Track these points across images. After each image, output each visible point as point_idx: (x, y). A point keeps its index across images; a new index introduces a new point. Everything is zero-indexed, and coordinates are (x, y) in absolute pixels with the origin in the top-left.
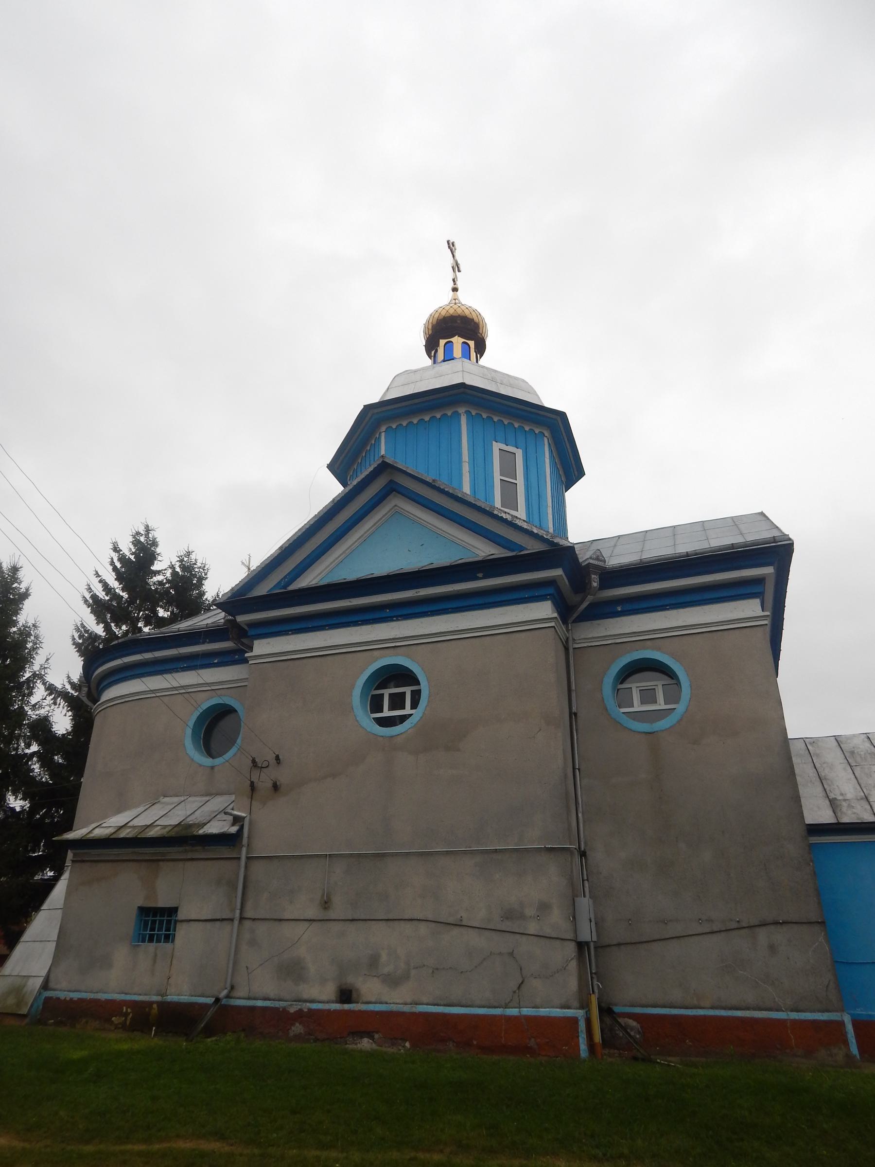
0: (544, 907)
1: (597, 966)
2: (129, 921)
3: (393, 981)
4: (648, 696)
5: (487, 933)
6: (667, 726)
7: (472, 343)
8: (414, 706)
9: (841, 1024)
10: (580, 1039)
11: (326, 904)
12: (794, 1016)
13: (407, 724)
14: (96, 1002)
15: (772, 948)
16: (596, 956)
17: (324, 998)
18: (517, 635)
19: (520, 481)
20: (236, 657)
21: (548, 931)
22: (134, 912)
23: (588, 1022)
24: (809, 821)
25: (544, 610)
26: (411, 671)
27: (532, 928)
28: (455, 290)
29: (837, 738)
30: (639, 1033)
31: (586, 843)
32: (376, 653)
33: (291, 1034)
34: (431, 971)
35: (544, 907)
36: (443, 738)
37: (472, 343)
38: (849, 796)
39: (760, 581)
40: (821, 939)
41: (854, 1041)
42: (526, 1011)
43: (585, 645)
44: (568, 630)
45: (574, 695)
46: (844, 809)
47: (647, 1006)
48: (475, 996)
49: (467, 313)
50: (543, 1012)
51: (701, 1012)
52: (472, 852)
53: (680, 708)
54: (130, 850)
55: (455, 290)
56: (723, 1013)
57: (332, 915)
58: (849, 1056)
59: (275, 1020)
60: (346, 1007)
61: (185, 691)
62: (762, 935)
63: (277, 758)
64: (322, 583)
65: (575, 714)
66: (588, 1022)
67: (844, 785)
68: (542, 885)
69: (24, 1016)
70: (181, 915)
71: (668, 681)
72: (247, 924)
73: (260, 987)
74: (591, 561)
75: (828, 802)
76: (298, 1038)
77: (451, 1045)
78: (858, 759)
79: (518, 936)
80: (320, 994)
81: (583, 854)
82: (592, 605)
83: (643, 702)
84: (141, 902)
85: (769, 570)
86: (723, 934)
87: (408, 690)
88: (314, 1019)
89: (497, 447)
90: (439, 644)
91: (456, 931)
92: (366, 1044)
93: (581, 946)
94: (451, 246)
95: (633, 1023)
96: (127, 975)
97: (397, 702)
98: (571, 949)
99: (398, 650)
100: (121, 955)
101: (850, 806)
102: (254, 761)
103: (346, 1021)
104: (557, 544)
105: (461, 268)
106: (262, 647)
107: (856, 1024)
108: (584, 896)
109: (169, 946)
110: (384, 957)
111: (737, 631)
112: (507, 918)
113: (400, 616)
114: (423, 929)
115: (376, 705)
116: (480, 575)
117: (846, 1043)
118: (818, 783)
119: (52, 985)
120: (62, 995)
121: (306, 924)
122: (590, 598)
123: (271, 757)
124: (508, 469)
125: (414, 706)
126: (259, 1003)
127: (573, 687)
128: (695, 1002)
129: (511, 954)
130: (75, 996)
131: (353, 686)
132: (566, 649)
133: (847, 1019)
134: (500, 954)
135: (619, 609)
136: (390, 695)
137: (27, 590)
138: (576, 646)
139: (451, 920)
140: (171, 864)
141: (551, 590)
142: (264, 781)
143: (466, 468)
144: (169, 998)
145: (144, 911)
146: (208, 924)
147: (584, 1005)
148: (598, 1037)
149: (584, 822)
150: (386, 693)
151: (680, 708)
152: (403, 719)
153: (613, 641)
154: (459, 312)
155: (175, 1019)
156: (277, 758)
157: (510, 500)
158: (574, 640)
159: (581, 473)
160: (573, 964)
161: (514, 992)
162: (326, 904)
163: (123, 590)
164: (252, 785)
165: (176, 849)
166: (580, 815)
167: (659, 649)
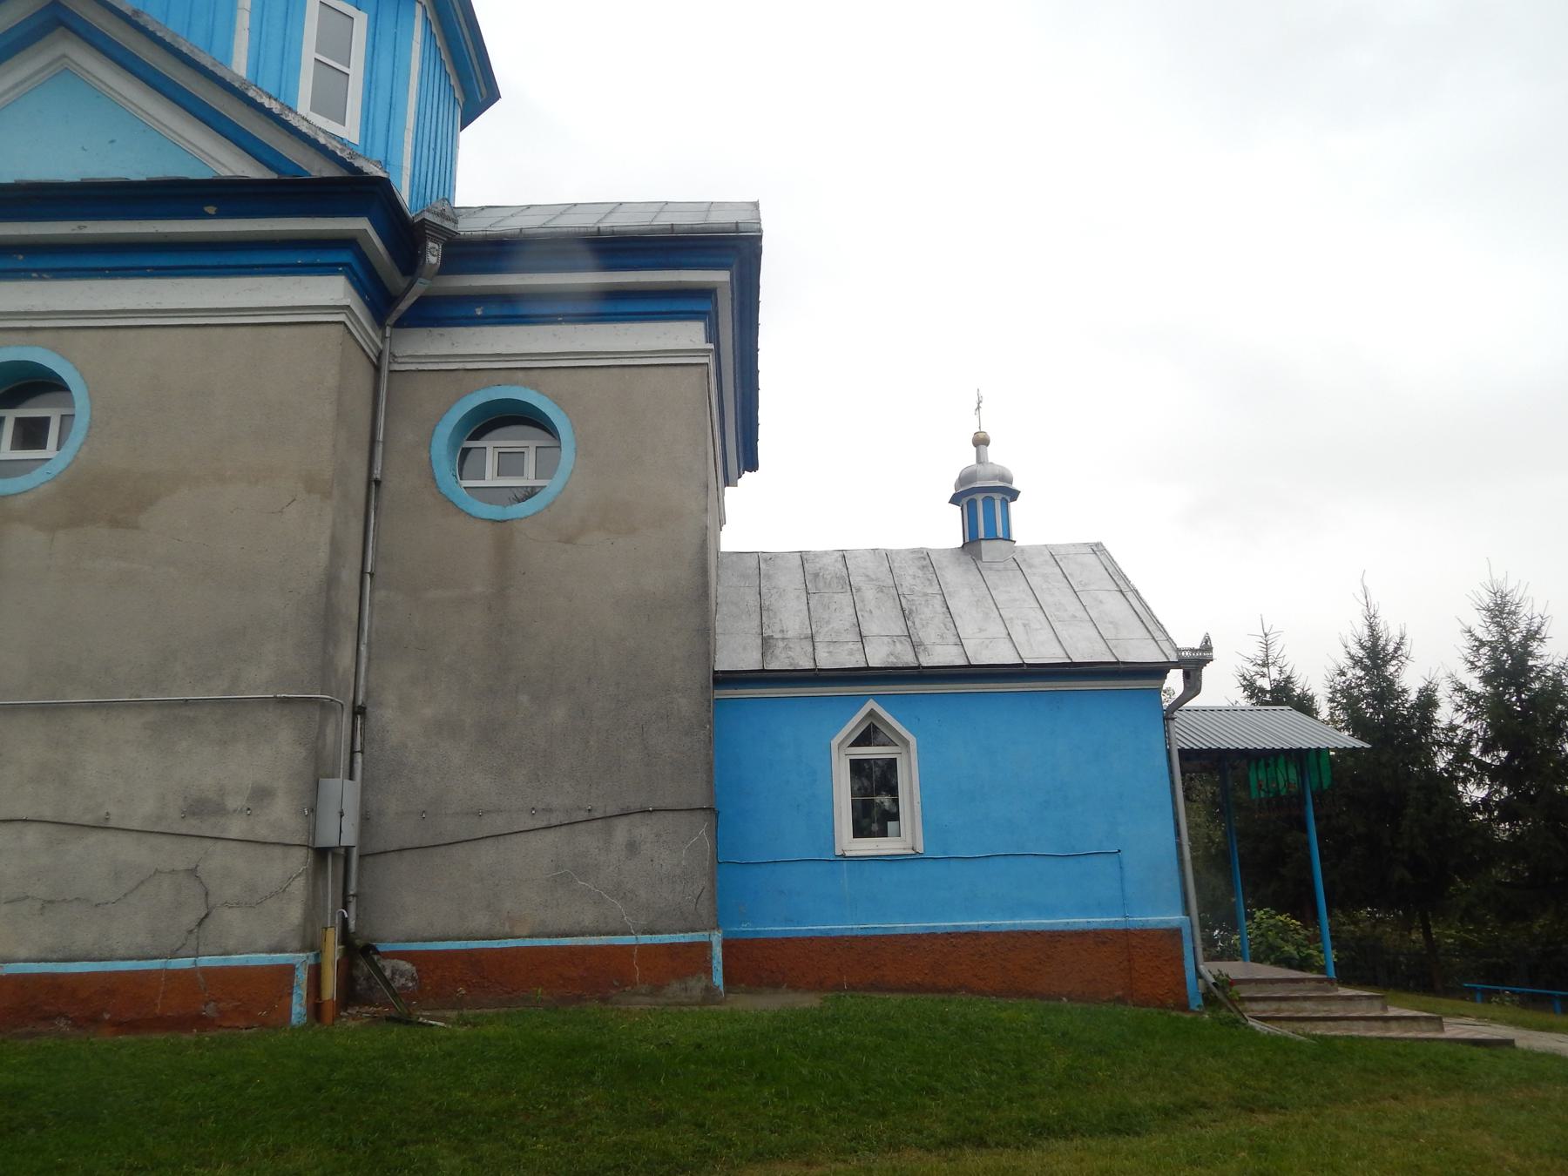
0: (261, 795)
1: (359, 883)
4: (511, 462)
5: (152, 839)
6: (444, 490)
9: (706, 946)
10: (295, 999)
12: (646, 939)
15: (632, 847)
18: (274, 330)
19: (356, 70)
21: (263, 833)
23: (316, 973)
24: (722, 665)
25: (333, 290)
26: (60, 378)
27: (236, 828)
29: (803, 557)
30: (413, 979)
31: (367, 694)
34: (38, 905)
35: (261, 795)
38: (790, 634)
39: (706, 293)
40: (702, 832)
41: (720, 968)
42: (205, 961)
43: (413, 367)
44: (383, 338)
45: (379, 449)
46: (777, 652)
47: (431, 940)
50: (236, 960)
52: (141, 705)
53: (553, 486)
56: (546, 942)
58: (709, 989)
62: (621, 829)
65: (378, 483)
66: (316, 973)
67: (790, 618)
68: (263, 761)
71: (544, 439)
74: (429, 217)
75: (759, 641)
77: (62, 1024)
78: (821, 585)
79: (208, 843)
81: (359, 711)
82: (423, 301)
83: (500, 473)
85: (721, 277)
86: (563, 829)
90: (121, 333)
91: (94, 838)
93: (321, 854)
95: (406, 966)
98: (299, 860)
99: (39, 336)
101: (787, 648)
104: (359, 170)
107: (727, 945)
108: (351, 777)
111: (661, 370)
112: (194, 814)
113: (35, 271)
114: (32, 836)
116: (211, 210)
117: (708, 971)
118: (756, 617)
122: (421, 287)
127: (381, 437)
128: (507, 929)
129: (193, 872)
132: (377, 369)
133: (716, 939)
134: (173, 871)
135: (479, 312)
136: (19, 421)
138: (396, 367)
139: (87, 819)
141: (345, 257)
143: (244, 20)
147: (313, 945)
148: (330, 989)
149: (369, 659)
151: (553, 486)
153: (460, 366)
157: (332, 105)
158: (393, 355)
159: (492, 95)
160: (299, 887)
161: (191, 932)
166: (363, 648)
167: (535, 386)
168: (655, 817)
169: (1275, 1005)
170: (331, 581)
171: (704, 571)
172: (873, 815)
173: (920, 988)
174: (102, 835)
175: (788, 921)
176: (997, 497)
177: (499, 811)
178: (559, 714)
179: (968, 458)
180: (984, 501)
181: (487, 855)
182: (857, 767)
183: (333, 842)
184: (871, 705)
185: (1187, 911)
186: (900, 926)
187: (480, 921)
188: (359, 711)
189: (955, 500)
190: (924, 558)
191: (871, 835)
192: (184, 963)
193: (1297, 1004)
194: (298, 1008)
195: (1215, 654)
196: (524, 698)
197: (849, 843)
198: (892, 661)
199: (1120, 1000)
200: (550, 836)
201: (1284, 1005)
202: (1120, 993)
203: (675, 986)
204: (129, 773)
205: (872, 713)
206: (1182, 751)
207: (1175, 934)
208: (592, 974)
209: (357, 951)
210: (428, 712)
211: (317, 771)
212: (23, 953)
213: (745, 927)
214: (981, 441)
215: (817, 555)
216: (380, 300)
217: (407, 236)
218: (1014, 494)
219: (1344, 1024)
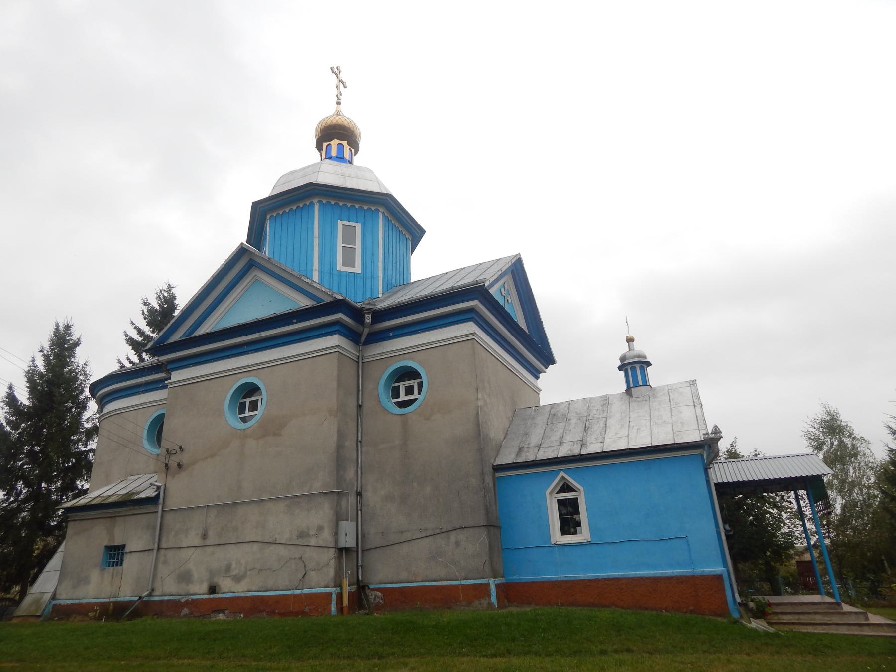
0: (320, 528)
1: (362, 561)
2: (98, 553)
3: (238, 579)
7: (345, 143)
8: (419, 393)
11: (205, 536)
12: (464, 582)
13: (253, 421)
14: (80, 605)
15: (457, 543)
16: (363, 555)
17: (201, 592)
19: (358, 246)
20: (159, 385)
21: (321, 543)
22: (102, 548)
23: (340, 596)
25: (334, 340)
27: (313, 541)
28: (339, 103)
32: (239, 375)
33: (182, 614)
35: (320, 528)
36: (271, 429)
37: (353, 150)
39: (471, 310)
40: (484, 535)
42: (306, 591)
48: (280, 584)
49: (346, 123)
50: (314, 591)
51: (415, 584)
52: (284, 498)
54: (100, 511)
55: (339, 103)
57: (208, 542)
58: (490, 604)
59: (173, 607)
60: (212, 596)
61: (135, 408)
62: (453, 536)
63: (181, 447)
64: (215, 330)
65: (360, 406)
66: (340, 596)
68: (318, 516)
69: (39, 616)
70: (127, 549)
72: (162, 551)
73: (168, 588)
76: (185, 616)
80: (199, 590)
81: (359, 494)
82: (370, 335)
84: (105, 543)
87: (414, 383)
88: (194, 604)
89: (341, 224)
91: (272, 547)
92: (221, 616)
94: (336, 72)
95: (379, 594)
96: (98, 587)
97: (409, 391)
98: (331, 553)
100: (95, 576)
102: (167, 451)
103: (213, 604)
105: (347, 84)
106: (176, 376)
109: (120, 568)
110: (234, 566)
114: (255, 547)
115: (396, 393)
116: (295, 321)
117: (489, 596)
119: (57, 597)
120: (62, 602)
121: (193, 549)
123: (177, 448)
124: (349, 236)
125: (419, 393)
126: (166, 598)
130: (69, 602)
131: (225, 398)
137: (79, 340)
139: (270, 540)
140: (122, 518)
141: (337, 328)
142: (173, 461)
143: (316, 241)
144: (119, 599)
145: (109, 548)
146: (142, 554)
148: (346, 602)
150: (248, 400)
152: (412, 401)
154: (340, 122)
155: (117, 611)
156: (181, 447)
157: (349, 260)
159: (422, 232)
162: (205, 536)
163: (153, 332)
164: (166, 465)
165: (125, 509)
166: (359, 470)
167: (412, 359)
168: (466, 530)
169: (796, 617)
170: (340, 447)
171: (478, 425)
172: (569, 524)
173: (594, 605)
174: (275, 545)
175: (534, 575)
176: (638, 367)
177: (408, 531)
178: (428, 489)
179: (624, 349)
180: (634, 368)
181: (405, 549)
182: (560, 502)
183: (344, 546)
184: (562, 474)
185: (725, 565)
186: (582, 576)
187: (404, 576)
188: (359, 494)
189: (620, 368)
190: (606, 401)
191: (569, 533)
192: (298, 592)
193: (811, 616)
194: (333, 608)
195: (723, 434)
196: (415, 484)
197: (557, 537)
198: (570, 454)
199: (691, 612)
200: (428, 540)
201: (802, 617)
202: (692, 608)
203: (476, 603)
204: (281, 523)
205: (563, 478)
206: (718, 485)
207: (719, 578)
208: (445, 597)
209: (362, 588)
210: (383, 493)
211: (339, 517)
212: (254, 589)
213: (515, 577)
214: (630, 340)
215: (558, 405)
216: (354, 336)
217: (357, 313)
218: (648, 364)
219: (833, 627)
